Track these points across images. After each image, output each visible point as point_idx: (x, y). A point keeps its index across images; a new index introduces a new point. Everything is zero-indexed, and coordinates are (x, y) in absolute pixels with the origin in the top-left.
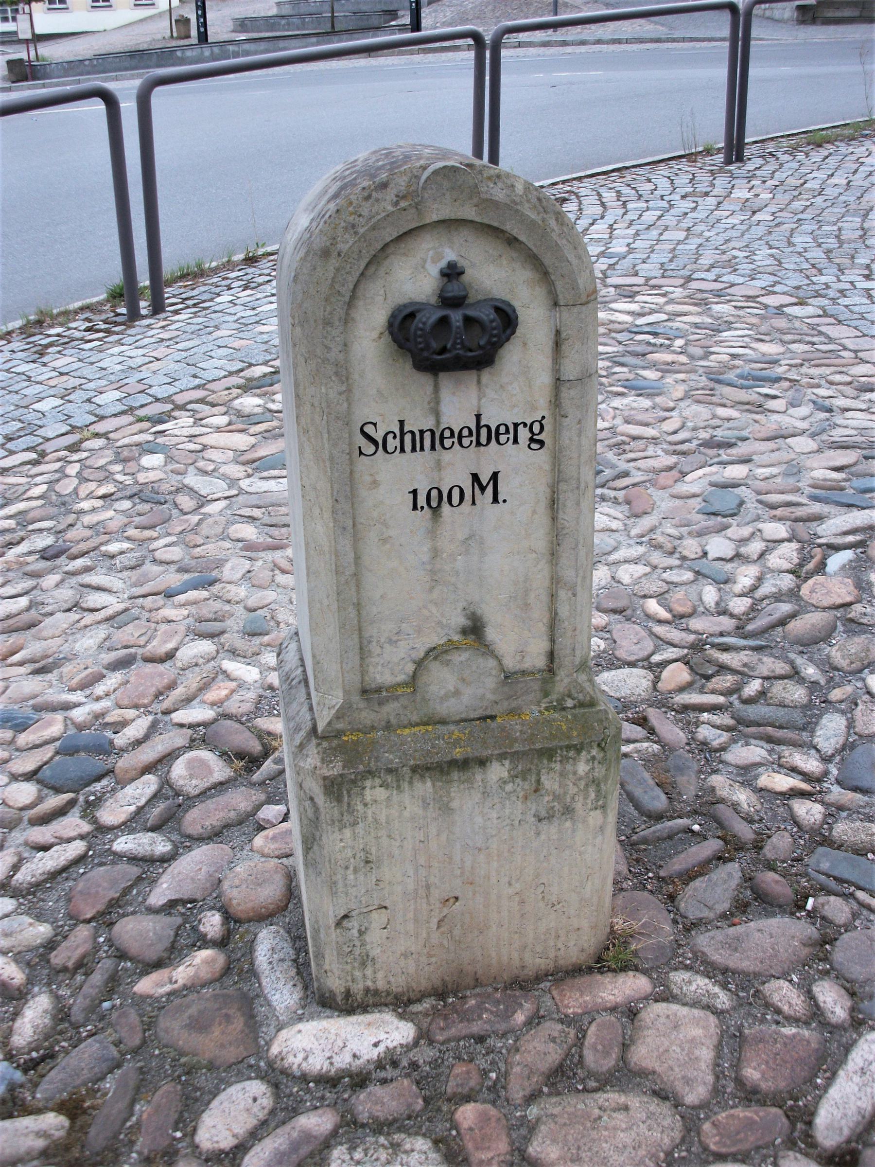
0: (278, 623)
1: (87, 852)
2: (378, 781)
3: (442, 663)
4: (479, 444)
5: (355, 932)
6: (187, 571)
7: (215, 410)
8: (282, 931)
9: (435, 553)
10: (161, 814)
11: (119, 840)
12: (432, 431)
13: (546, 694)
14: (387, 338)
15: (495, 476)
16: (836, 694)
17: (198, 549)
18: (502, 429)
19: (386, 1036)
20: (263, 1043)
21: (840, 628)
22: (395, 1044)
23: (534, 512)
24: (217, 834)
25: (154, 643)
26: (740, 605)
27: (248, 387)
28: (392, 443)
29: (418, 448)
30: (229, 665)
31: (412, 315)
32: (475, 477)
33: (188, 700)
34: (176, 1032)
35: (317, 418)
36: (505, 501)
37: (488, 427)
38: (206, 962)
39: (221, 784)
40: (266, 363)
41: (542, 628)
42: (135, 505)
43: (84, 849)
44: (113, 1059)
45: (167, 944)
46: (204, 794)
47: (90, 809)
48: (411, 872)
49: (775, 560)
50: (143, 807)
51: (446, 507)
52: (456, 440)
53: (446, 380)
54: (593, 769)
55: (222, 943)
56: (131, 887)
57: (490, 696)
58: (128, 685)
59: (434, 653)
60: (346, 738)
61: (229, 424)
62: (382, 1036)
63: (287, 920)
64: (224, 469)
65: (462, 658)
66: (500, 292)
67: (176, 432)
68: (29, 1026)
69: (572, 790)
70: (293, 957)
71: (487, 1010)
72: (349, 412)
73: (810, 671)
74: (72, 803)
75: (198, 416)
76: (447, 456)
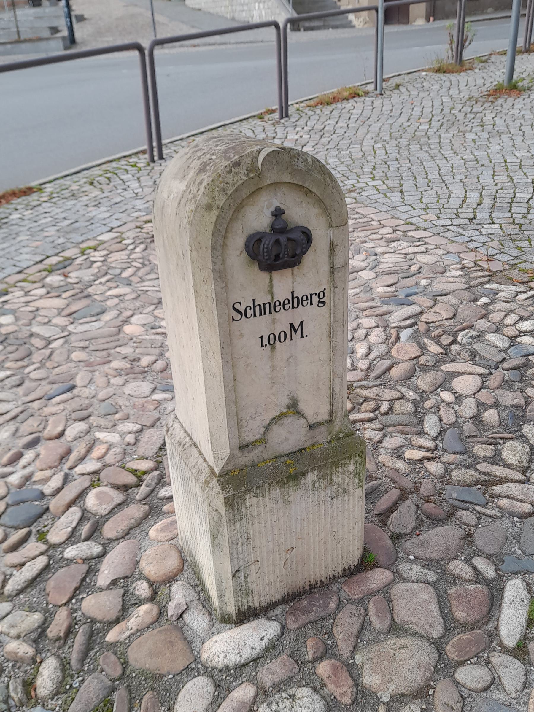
0: (120, 407)
1: (49, 562)
2: (252, 494)
3: (279, 425)
4: (293, 307)
5: (243, 578)
6: (54, 383)
7: (36, 285)
8: (185, 583)
9: (273, 368)
10: (89, 530)
11: (67, 550)
12: (270, 303)
13: (330, 433)
14: (245, 254)
15: (302, 323)
16: (428, 404)
17: (56, 369)
18: (305, 298)
19: (266, 632)
20: (196, 653)
21: (418, 370)
22: (272, 636)
23: (321, 340)
24: (128, 534)
25: (49, 428)
26: (363, 364)
27: (50, 271)
28: (250, 312)
30: (98, 435)
31: (259, 240)
32: (292, 325)
33: (82, 459)
34: (143, 660)
35: (210, 303)
37: (298, 298)
38: (147, 612)
39: (119, 504)
40: (56, 255)
41: (326, 399)
42: (5, 347)
43: (47, 560)
44: (109, 686)
45: (120, 607)
46: (112, 512)
47: (42, 536)
48: (270, 539)
49: (373, 338)
50: (76, 527)
51: (277, 342)
52: (282, 307)
53: (276, 275)
54: (356, 467)
55: (153, 598)
56: (85, 577)
57: (303, 439)
58: (41, 456)
59: (274, 420)
60: (232, 474)
61: (48, 293)
62: (264, 633)
63: (186, 576)
64: (54, 321)
65: (289, 421)
67: (16, 301)
68: (48, 680)
69: (347, 480)
70: (197, 598)
71: (314, 605)
72: (227, 298)
73: (411, 394)
74: (29, 534)
75: (26, 290)
76: (277, 316)
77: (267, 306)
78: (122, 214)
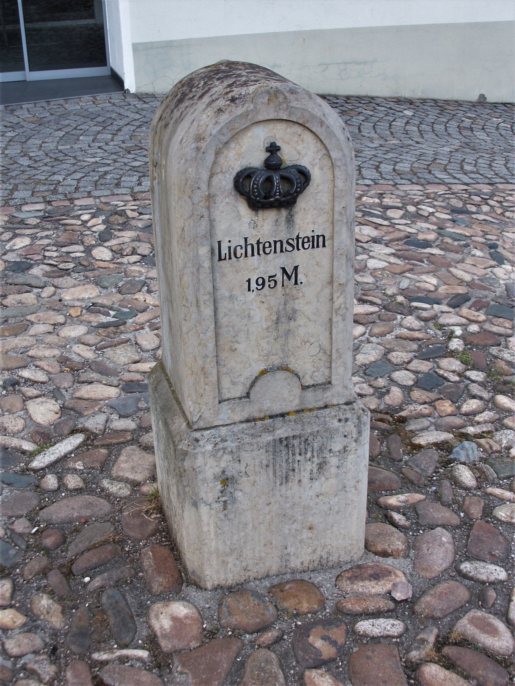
15: (296, 268)
29: (315, 246)
31: (249, 177)
32: (284, 270)
36: (301, 283)
66: (305, 162)
77: (321, 239)
78: (193, 118)
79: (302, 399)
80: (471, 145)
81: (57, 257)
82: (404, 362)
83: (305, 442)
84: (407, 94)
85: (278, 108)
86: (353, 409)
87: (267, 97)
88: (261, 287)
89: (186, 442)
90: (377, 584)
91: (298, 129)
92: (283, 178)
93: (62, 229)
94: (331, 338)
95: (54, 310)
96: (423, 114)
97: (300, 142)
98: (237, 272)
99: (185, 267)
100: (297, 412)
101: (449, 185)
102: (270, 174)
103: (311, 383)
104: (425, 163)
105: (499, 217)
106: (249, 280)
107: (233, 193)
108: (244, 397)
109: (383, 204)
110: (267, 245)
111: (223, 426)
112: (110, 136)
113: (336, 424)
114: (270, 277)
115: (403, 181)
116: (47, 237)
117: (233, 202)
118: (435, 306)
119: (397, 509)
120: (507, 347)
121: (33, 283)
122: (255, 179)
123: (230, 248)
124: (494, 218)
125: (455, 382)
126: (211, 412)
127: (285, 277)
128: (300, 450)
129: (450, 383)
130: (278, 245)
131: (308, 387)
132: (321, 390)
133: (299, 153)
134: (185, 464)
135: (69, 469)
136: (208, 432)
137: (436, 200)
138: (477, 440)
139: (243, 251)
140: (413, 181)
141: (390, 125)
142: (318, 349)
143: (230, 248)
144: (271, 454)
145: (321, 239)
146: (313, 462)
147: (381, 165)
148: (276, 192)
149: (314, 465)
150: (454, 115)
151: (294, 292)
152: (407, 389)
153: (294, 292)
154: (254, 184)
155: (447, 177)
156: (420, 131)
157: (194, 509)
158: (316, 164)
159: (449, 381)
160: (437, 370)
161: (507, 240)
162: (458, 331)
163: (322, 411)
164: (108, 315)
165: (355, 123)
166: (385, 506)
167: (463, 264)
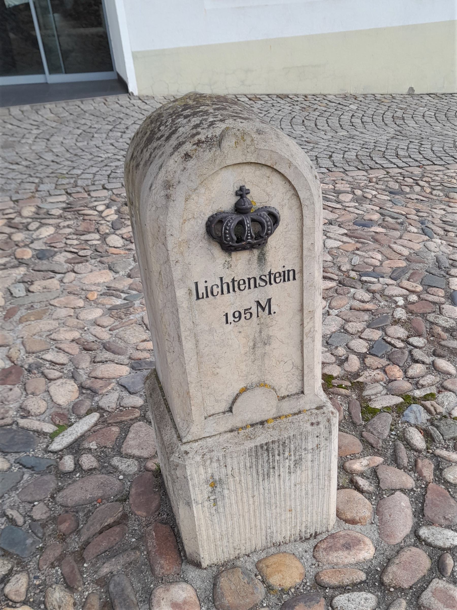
15: (269, 301)
31: (221, 222)
32: (258, 303)
77: (291, 273)
79: (278, 409)
80: (403, 132)
81: (77, 245)
82: (358, 331)
83: (282, 445)
84: (351, 91)
85: (246, 151)
86: (324, 413)
87: (234, 140)
88: (238, 319)
89: (177, 455)
90: (349, 554)
91: (268, 172)
92: (253, 220)
93: (81, 218)
94: (303, 356)
95: (74, 294)
96: (365, 108)
97: (269, 184)
98: (215, 308)
99: (165, 307)
100: (275, 419)
101: (387, 170)
102: (241, 219)
103: (286, 393)
104: (367, 150)
105: (428, 196)
106: (227, 314)
107: (206, 237)
108: (227, 411)
109: (336, 189)
110: (242, 282)
111: (210, 437)
112: (119, 134)
113: (310, 428)
114: (245, 310)
115: (351, 168)
116: (68, 226)
117: (207, 245)
118: (381, 279)
119: (362, 475)
120: (441, 313)
121: (57, 270)
122: (227, 225)
123: (206, 287)
124: (423, 197)
125: (400, 348)
126: (198, 427)
127: (260, 309)
128: (279, 452)
129: (396, 349)
130: (252, 281)
131: (283, 398)
132: (295, 400)
133: (268, 195)
134: (178, 472)
135: (84, 449)
136: (197, 444)
137: (377, 184)
138: (423, 402)
139: (219, 289)
140: (359, 167)
141: (340, 118)
142: (292, 366)
143: (206, 287)
144: (253, 458)
145: (291, 273)
146: (290, 460)
147: (334, 155)
148: (248, 236)
149: (291, 462)
150: (389, 107)
151: (268, 320)
152: (362, 357)
153: (268, 320)
154: (226, 229)
155: (385, 162)
156: (362, 122)
157: (187, 507)
158: (285, 205)
159: (395, 347)
160: (385, 338)
161: (434, 216)
162: (401, 302)
163: (296, 417)
164: (118, 297)
165: (311, 118)
166: (351, 471)
167: (401, 240)
